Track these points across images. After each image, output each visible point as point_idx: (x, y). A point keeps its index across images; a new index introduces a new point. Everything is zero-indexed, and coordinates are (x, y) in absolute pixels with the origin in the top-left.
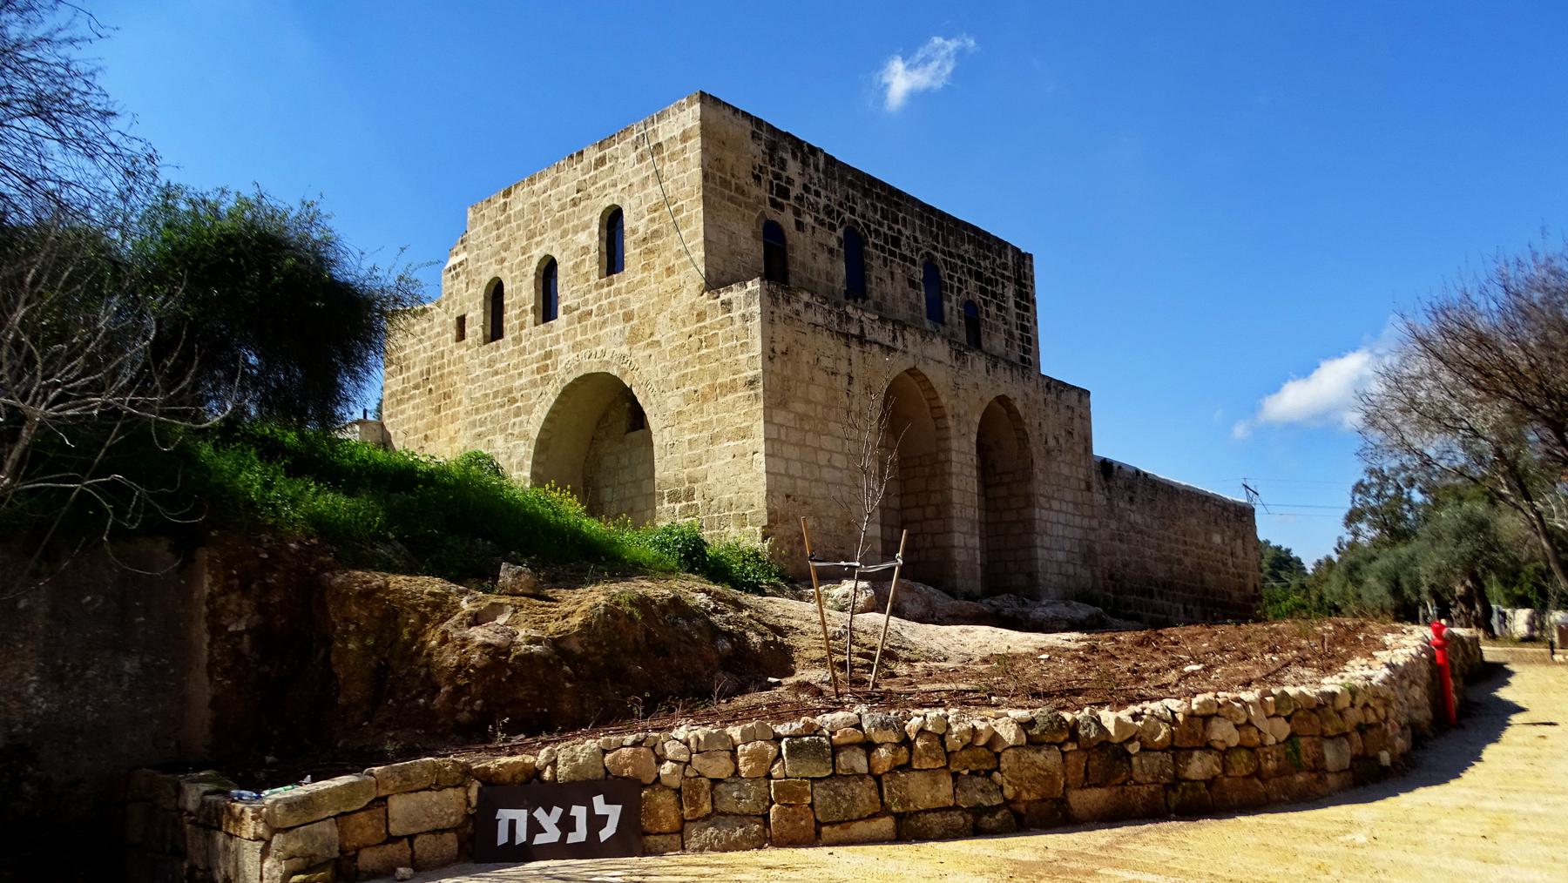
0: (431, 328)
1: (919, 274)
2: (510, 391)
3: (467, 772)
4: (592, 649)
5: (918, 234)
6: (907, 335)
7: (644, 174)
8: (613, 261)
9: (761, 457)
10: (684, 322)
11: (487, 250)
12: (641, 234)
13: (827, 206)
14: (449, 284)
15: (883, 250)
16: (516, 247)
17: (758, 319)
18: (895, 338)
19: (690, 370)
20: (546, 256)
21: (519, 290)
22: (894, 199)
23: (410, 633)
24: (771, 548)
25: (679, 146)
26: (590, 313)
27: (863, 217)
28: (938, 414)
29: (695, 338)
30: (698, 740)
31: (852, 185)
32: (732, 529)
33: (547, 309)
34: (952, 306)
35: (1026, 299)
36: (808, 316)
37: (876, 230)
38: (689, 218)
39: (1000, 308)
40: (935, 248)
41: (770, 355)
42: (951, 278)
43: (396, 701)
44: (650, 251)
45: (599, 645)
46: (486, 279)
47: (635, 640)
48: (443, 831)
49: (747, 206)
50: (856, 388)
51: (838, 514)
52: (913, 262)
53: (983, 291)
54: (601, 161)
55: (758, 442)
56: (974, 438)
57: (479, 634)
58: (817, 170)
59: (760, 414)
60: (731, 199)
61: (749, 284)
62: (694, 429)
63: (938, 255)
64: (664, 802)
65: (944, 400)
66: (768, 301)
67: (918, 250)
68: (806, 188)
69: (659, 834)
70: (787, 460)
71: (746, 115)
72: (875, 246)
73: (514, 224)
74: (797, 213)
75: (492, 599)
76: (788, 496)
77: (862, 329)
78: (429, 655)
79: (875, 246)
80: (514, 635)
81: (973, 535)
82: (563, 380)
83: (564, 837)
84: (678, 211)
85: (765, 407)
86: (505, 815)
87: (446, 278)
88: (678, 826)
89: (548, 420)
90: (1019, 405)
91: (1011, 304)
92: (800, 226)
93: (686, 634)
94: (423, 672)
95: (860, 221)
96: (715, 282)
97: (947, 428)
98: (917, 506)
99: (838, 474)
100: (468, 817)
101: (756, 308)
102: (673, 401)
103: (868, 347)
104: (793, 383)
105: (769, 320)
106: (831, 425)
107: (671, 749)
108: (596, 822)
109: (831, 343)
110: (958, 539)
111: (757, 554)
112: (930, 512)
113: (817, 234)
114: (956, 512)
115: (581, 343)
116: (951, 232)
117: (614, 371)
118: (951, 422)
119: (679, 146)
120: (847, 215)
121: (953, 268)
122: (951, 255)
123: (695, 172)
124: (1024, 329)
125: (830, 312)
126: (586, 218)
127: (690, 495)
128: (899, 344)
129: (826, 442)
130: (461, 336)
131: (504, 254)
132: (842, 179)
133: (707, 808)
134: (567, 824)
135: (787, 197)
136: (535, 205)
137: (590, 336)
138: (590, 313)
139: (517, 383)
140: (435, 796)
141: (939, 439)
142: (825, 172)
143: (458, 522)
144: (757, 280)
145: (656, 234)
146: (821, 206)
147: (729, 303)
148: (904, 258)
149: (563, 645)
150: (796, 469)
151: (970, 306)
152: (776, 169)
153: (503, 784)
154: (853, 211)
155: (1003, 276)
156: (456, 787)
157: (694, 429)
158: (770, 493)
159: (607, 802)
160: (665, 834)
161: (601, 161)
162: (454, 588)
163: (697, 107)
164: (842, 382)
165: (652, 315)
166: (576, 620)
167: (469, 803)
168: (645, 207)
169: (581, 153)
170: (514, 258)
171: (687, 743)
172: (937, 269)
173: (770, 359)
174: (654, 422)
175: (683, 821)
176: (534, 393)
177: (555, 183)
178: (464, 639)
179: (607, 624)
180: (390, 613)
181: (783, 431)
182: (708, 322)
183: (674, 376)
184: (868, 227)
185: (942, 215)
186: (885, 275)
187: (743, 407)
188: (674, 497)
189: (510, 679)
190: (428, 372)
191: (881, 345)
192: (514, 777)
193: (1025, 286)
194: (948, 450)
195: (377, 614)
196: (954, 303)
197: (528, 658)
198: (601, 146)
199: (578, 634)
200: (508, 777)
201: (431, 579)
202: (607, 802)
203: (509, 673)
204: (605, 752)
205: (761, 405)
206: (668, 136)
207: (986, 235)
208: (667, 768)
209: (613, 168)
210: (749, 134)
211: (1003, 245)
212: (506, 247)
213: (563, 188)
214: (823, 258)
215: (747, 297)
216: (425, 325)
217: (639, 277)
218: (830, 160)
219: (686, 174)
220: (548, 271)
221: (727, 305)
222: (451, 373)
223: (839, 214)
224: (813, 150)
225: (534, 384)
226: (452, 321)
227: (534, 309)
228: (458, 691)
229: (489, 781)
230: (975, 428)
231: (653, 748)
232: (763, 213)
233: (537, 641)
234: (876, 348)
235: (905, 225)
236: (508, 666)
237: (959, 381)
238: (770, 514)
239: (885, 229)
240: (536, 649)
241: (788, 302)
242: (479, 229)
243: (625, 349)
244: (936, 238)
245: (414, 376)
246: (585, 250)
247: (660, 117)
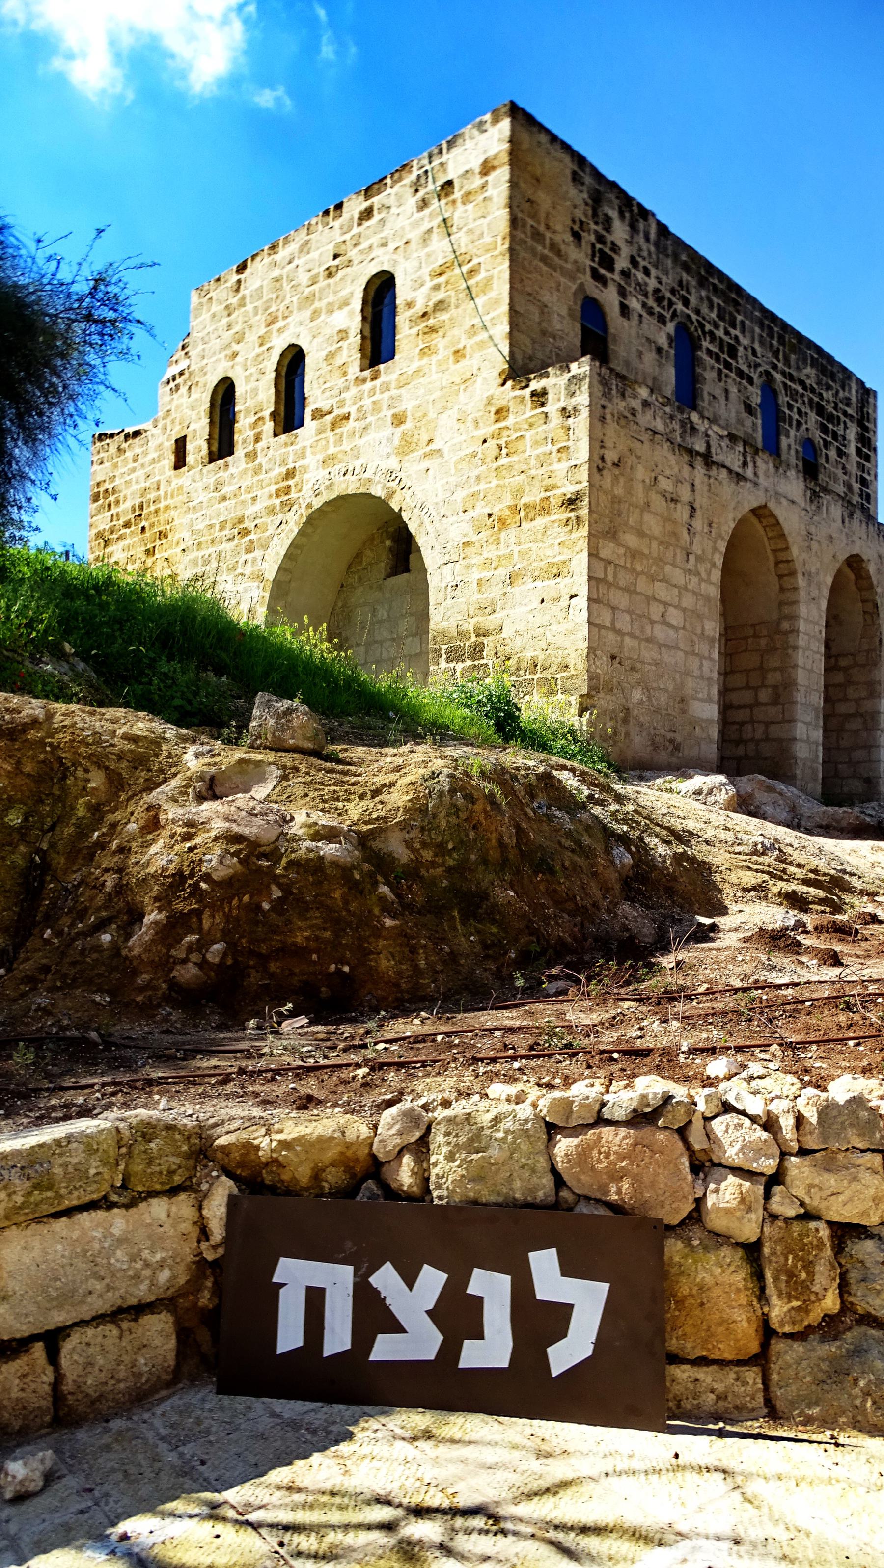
0: (146, 453)
2: (241, 521)
3: (201, 1150)
4: (428, 855)
5: (757, 346)
6: (759, 462)
7: (426, 226)
8: (378, 347)
9: (582, 602)
10: (476, 423)
11: (215, 344)
12: (419, 309)
13: (657, 291)
14: (167, 398)
16: (252, 337)
17: (585, 413)
18: (745, 464)
19: (482, 486)
20: (292, 346)
21: (255, 391)
22: (732, 296)
23: (90, 807)
24: (591, 723)
25: (478, 181)
26: (347, 417)
27: (698, 312)
28: (785, 570)
29: (492, 443)
30: (800, 1120)
31: (686, 267)
32: (536, 697)
33: (289, 413)
34: (789, 442)
35: (867, 446)
36: (645, 419)
38: (488, 281)
39: (841, 454)
40: (775, 367)
41: (598, 465)
42: (790, 407)
43: (58, 934)
44: (432, 330)
45: (440, 849)
46: (213, 380)
47: (501, 844)
48: (139, 1310)
49: (564, 273)
50: (698, 524)
51: (671, 688)
52: (751, 381)
53: (824, 429)
54: (367, 214)
55: (578, 580)
56: (824, 604)
57: (215, 815)
58: (647, 239)
59: (583, 544)
60: (544, 259)
61: (574, 366)
62: (488, 563)
63: (778, 377)
64: (715, 1280)
65: (795, 551)
66: (598, 389)
67: (757, 365)
68: (634, 261)
69: (702, 1362)
70: (614, 609)
71: (566, 147)
72: (709, 352)
73: (249, 307)
74: (622, 292)
75: (239, 754)
76: (613, 658)
77: (708, 446)
78: (123, 850)
79: (709, 352)
80: (286, 821)
82: (309, 506)
83: (450, 1350)
84: (472, 272)
85: (590, 535)
86: (294, 1274)
87: (164, 391)
88: (754, 1347)
89: (289, 556)
90: (872, 569)
91: (852, 450)
92: (625, 310)
93: (569, 834)
94: (110, 881)
95: (694, 317)
96: (519, 370)
97: (796, 589)
98: (748, 687)
99: (671, 633)
100: (201, 1265)
101: (583, 398)
102: (458, 529)
103: (714, 471)
104: (624, 507)
105: (598, 417)
106: (668, 568)
107: (734, 1139)
108: (538, 1322)
109: (672, 459)
110: (800, 730)
111: (572, 732)
112: (764, 695)
113: (645, 326)
114: (799, 697)
115: (333, 457)
116: (793, 349)
117: (378, 491)
118: (801, 582)
119: (478, 181)
120: (679, 307)
121: (794, 394)
122: (791, 378)
123: (500, 217)
124: (864, 482)
125: (672, 418)
126: (344, 293)
127: (477, 651)
128: (749, 473)
129: (661, 591)
130: (180, 462)
131: (235, 347)
132: (676, 257)
133: (831, 1302)
134: (458, 1316)
135: (611, 269)
136: (277, 280)
137: (346, 446)
138: (347, 417)
139: (250, 510)
140: (118, 1221)
141: (781, 604)
142: (657, 245)
143: (171, 656)
144: (586, 359)
145: (440, 306)
146: (650, 289)
147: (544, 393)
148: (740, 374)
149: (376, 845)
150: (624, 622)
151: (808, 444)
152: (599, 228)
153: (289, 1191)
155: (845, 414)
156: (173, 1192)
157: (488, 563)
158: (592, 650)
159: (567, 1270)
160: (721, 1363)
161: (367, 214)
162: (171, 731)
163: (505, 124)
164: (682, 513)
165: (432, 415)
166: (398, 798)
167: (204, 1233)
168: (426, 271)
169: (339, 206)
170: (248, 350)
171: (770, 1124)
172: (775, 393)
173: (600, 470)
174: (431, 557)
175: (767, 1332)
176: (271, 522)
177: (305, 247)
178: (190, 824)
179: (456, 810)
180: (53, 773)
181: (610, 569)
182: (510, 421)
183: (460, 495)
184: (702, 326)
185: (785, 326)
186: (718, 392)
187: (559, 534)
188: (455, 655)
189: (278, 906)
190: (141, 508)
191: (730, 471)
192: (317, 1175)
193: (867, 429)
194: (793, 617)
195: (28, 768)
196: (791, 441)
197: (315, 867)
198: (368, 192)
199: (404, 826)
200: (303, 1174)
201: (130, 714)
202: (567, 1270)
203: (277, 893)
204: (552, 1129)
205: (584, 531)
206: (461, 171)
207: (830, 359)
208: (725, 1194)
209: (382, 221)
210: (568, 172)
211: (848, 375)
212: (239, 338)
213: (314, 255)
214: (650, 357)
215: (570, 386)
216: (138, 450)
217: (415, 366)
218: (663, 229)
219: (485, 220)
220: (293, 363)
221: (540, 397)
222: (167, 508)
223: (671, 304)
224: (645, 213)
225: (272, 511)
226: (170, 445)
227: (274, 415)
228: (171, 930)
229: (255, 1180)
230: (826, 592)
231: (682, 1132)
232: (582, 285)
233: (330, 835)
234: (724, 473)
235: (743, 331)
236: (275, 879)
237: (813, 529)
238: (590, 679)
240: (329, 849)
241: (623, 395)
242: (206, 316)
243: (393, 463)
244: (776, 354)
245: (125, 512)
246: (343, 334)
247: (451, 144)
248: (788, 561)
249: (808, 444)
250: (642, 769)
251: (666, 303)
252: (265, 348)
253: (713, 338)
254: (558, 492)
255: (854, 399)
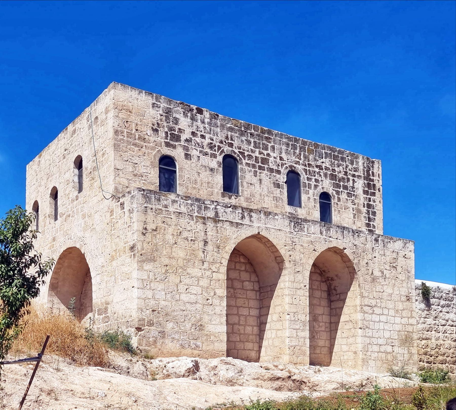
1: (282, 178)
15: (254, 166)
18: (243, 217)
37: (249, 156)
39: (349, 195)
50: (210, 247)
60: (135, 145)
67: (282, 165)
74: (186, 148)
77: (217, 213)
81: (303, 330)
95: (237, 151)
102: (101, 260)
103: (220, 225)
125: (192, 205)
142: (210, 124)
148: (271, 170)
154: (231, 145)
184: (242, 154)
223: (219, 148)
234: (227, 225)
239: (257, 154)
244: (299, 157)
248: (280, 256)
249: (325, 196)
250: (115, 348)
251: (216, 148)
252: (46, 188)
253: (250, 157)
254: (128, 244)
255: (361, 168)
